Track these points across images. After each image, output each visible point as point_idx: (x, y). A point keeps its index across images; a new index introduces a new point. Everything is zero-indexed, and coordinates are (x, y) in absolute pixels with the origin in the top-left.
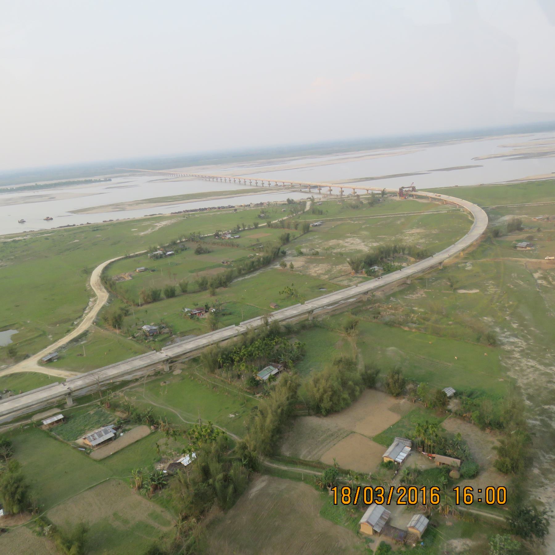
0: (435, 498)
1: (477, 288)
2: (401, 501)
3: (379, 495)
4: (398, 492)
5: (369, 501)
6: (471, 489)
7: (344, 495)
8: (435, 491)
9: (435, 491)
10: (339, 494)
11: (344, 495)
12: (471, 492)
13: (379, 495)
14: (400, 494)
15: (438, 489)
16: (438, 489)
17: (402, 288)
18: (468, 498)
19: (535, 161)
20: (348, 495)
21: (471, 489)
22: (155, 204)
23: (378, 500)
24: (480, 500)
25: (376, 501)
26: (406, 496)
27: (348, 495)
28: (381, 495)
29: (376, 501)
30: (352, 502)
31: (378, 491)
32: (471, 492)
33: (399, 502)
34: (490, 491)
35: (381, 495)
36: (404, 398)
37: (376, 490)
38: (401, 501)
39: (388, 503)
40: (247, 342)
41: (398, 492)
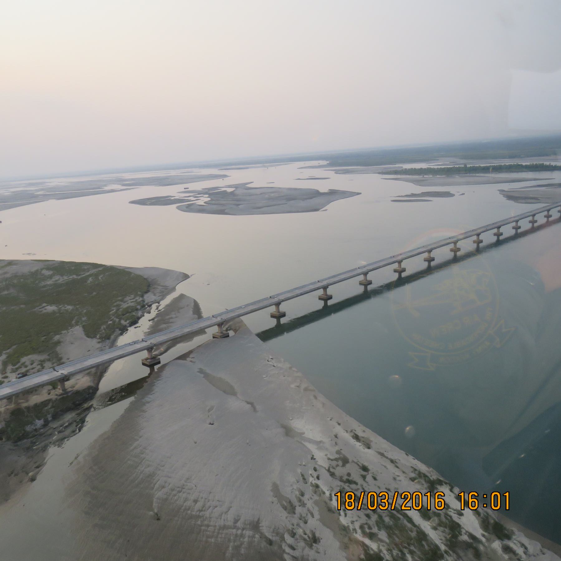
0: (473, 503)
2: (405, 507)
3: (383, 501)
4: (403, 497)
5: (373, 507)
6: (443, 495)
7: (348, 501)
10: (433, 500)
11: (348, 501)
12: (442, 497)
13: (383, 501)
15: (476, 495)
16: (476, 495)
17: (86, 406)
19: (537, 177)
20: (352, 501)
21: (443, 495)
22: (524, 201)
23: (382, 505)
24: (485, 505)
26: (411, 500)
27: (352, 501)
28: (385, 501)
30: (356, 508)
31: (382, 496)
32: (442, 497)
33: (403, 508)
34: (417, 496)
35: (385, 501)
37: (380, 495)
38: (405, 507)
39: (359, 508)
41: (403, 497)
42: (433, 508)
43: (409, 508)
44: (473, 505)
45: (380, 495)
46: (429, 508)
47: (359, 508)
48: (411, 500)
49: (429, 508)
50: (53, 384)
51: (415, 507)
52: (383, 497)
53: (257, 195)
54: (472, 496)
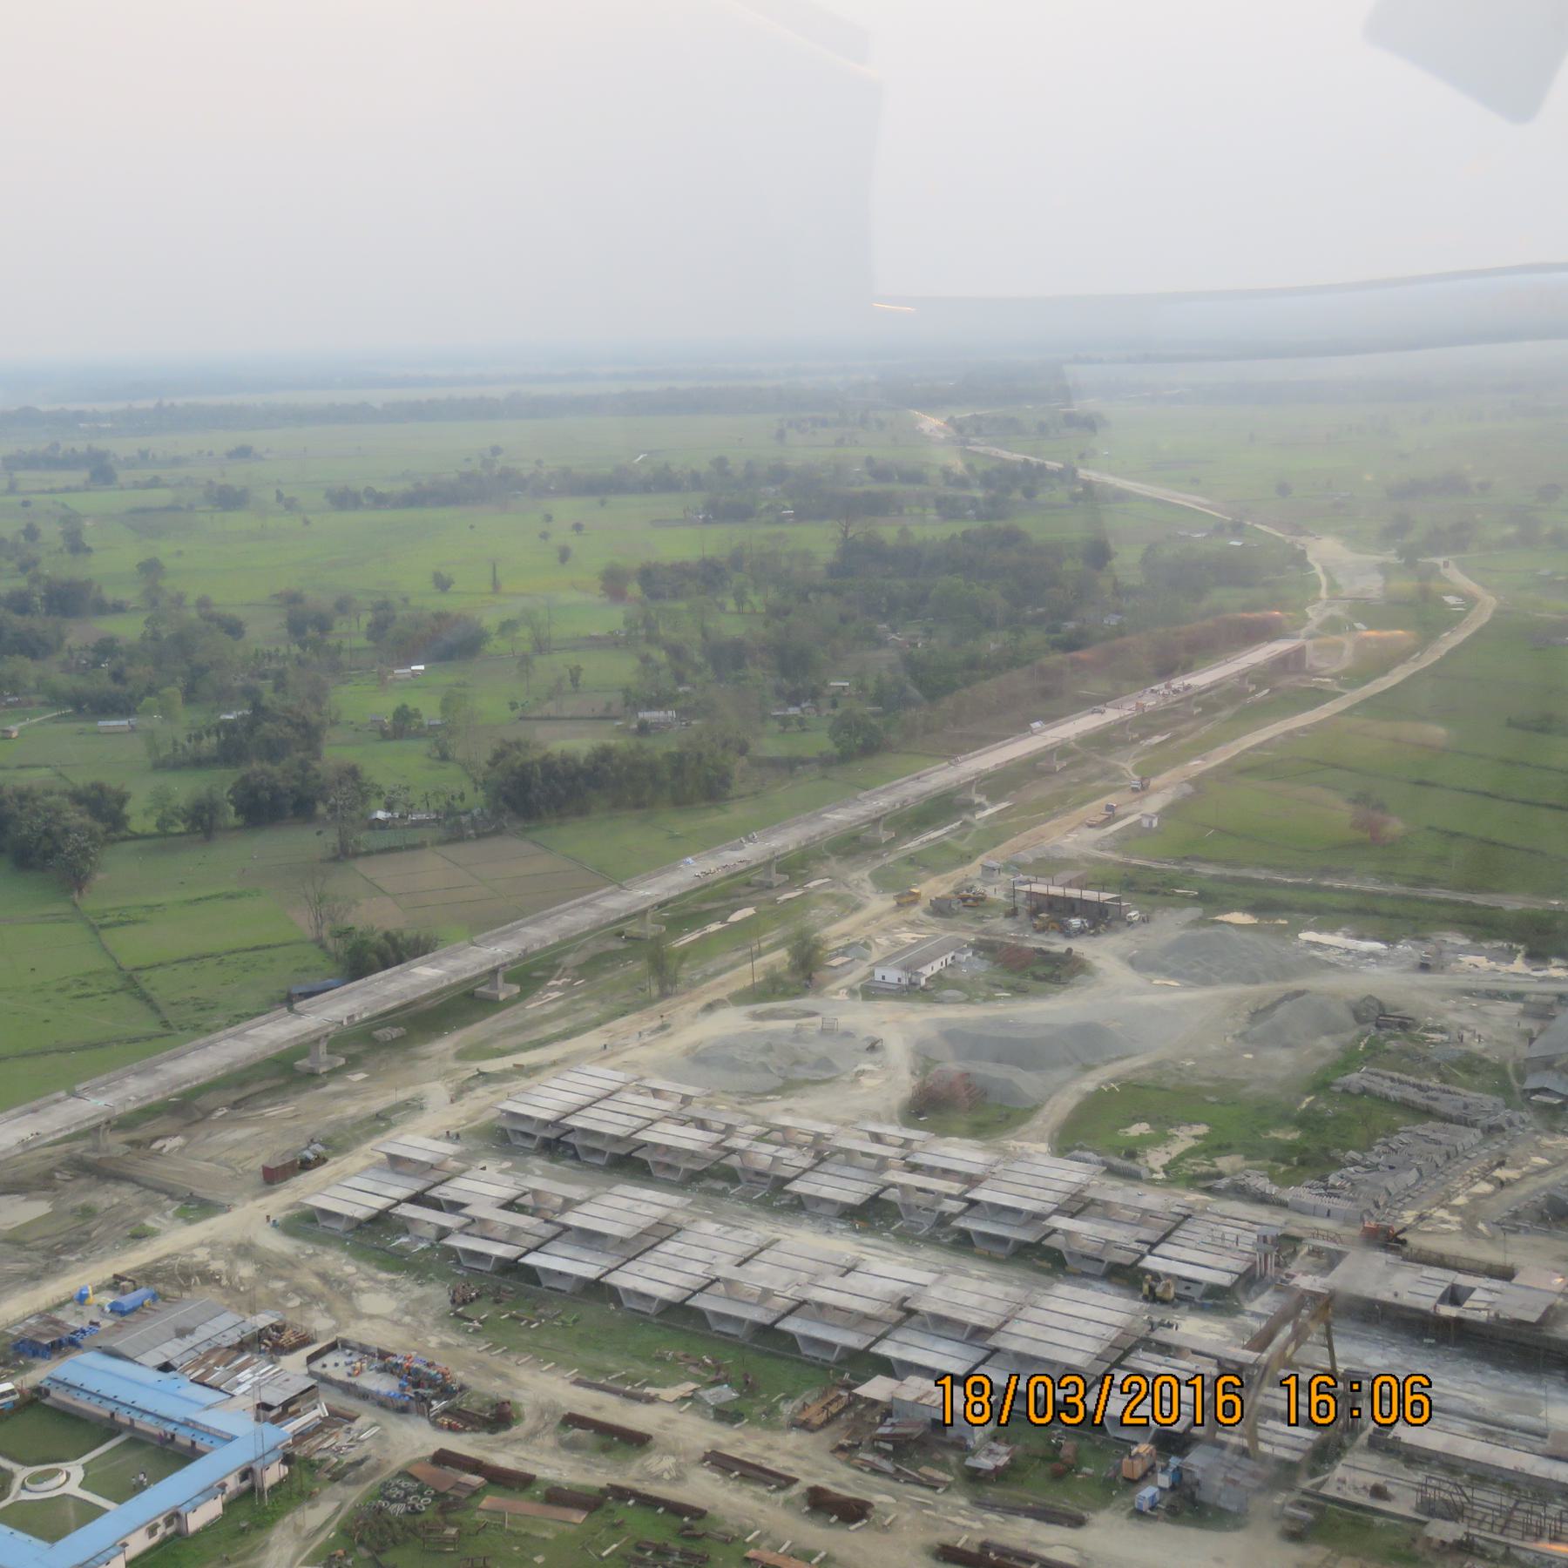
0: (1323, 1405)
1: (1402, 628)
4: (1126, 1389)
5: (1043, 1416)
6: (1426, 1383)
7: (972, 1399)
8: (1417, 1388)
9: (1417, 1388)
10: (1303, 1398)
11: (972, 1399)
13: (1070, 1400)
14: (1130, 1397)
18: (1323, 1405)
20: (984, 1399)
21: (1426, 1383)
25: (1063, 1415)
26: (1149, 1398)
27: (984, 1399)
28: (1076, 1400)
29: (1063, 1415)
33: (1127, 1420)
36: (393, 1288)
37: (1063, 1384)
39: (1003, 1421)
40: (938, 1067)
41: (1126, 1389)
42: (959, 1421)
43: (1144, 1421)
44: (1417, 1410)
45: (1063, 1384)
46: (948, 1421)
47: (1003, 1421)
48: (1149, 1398)
49: (948, 1421)
50: (760, 954)
51: (1159, 1418)
52: (1071, 1390)
53: (380, 501)
54: (973, 1385)
